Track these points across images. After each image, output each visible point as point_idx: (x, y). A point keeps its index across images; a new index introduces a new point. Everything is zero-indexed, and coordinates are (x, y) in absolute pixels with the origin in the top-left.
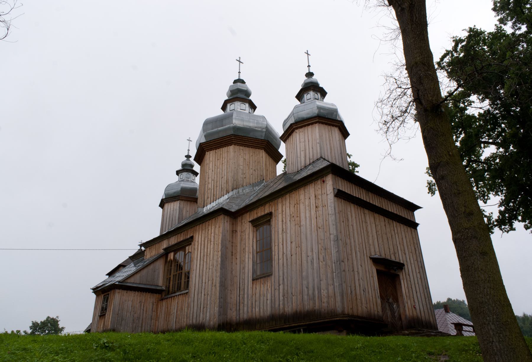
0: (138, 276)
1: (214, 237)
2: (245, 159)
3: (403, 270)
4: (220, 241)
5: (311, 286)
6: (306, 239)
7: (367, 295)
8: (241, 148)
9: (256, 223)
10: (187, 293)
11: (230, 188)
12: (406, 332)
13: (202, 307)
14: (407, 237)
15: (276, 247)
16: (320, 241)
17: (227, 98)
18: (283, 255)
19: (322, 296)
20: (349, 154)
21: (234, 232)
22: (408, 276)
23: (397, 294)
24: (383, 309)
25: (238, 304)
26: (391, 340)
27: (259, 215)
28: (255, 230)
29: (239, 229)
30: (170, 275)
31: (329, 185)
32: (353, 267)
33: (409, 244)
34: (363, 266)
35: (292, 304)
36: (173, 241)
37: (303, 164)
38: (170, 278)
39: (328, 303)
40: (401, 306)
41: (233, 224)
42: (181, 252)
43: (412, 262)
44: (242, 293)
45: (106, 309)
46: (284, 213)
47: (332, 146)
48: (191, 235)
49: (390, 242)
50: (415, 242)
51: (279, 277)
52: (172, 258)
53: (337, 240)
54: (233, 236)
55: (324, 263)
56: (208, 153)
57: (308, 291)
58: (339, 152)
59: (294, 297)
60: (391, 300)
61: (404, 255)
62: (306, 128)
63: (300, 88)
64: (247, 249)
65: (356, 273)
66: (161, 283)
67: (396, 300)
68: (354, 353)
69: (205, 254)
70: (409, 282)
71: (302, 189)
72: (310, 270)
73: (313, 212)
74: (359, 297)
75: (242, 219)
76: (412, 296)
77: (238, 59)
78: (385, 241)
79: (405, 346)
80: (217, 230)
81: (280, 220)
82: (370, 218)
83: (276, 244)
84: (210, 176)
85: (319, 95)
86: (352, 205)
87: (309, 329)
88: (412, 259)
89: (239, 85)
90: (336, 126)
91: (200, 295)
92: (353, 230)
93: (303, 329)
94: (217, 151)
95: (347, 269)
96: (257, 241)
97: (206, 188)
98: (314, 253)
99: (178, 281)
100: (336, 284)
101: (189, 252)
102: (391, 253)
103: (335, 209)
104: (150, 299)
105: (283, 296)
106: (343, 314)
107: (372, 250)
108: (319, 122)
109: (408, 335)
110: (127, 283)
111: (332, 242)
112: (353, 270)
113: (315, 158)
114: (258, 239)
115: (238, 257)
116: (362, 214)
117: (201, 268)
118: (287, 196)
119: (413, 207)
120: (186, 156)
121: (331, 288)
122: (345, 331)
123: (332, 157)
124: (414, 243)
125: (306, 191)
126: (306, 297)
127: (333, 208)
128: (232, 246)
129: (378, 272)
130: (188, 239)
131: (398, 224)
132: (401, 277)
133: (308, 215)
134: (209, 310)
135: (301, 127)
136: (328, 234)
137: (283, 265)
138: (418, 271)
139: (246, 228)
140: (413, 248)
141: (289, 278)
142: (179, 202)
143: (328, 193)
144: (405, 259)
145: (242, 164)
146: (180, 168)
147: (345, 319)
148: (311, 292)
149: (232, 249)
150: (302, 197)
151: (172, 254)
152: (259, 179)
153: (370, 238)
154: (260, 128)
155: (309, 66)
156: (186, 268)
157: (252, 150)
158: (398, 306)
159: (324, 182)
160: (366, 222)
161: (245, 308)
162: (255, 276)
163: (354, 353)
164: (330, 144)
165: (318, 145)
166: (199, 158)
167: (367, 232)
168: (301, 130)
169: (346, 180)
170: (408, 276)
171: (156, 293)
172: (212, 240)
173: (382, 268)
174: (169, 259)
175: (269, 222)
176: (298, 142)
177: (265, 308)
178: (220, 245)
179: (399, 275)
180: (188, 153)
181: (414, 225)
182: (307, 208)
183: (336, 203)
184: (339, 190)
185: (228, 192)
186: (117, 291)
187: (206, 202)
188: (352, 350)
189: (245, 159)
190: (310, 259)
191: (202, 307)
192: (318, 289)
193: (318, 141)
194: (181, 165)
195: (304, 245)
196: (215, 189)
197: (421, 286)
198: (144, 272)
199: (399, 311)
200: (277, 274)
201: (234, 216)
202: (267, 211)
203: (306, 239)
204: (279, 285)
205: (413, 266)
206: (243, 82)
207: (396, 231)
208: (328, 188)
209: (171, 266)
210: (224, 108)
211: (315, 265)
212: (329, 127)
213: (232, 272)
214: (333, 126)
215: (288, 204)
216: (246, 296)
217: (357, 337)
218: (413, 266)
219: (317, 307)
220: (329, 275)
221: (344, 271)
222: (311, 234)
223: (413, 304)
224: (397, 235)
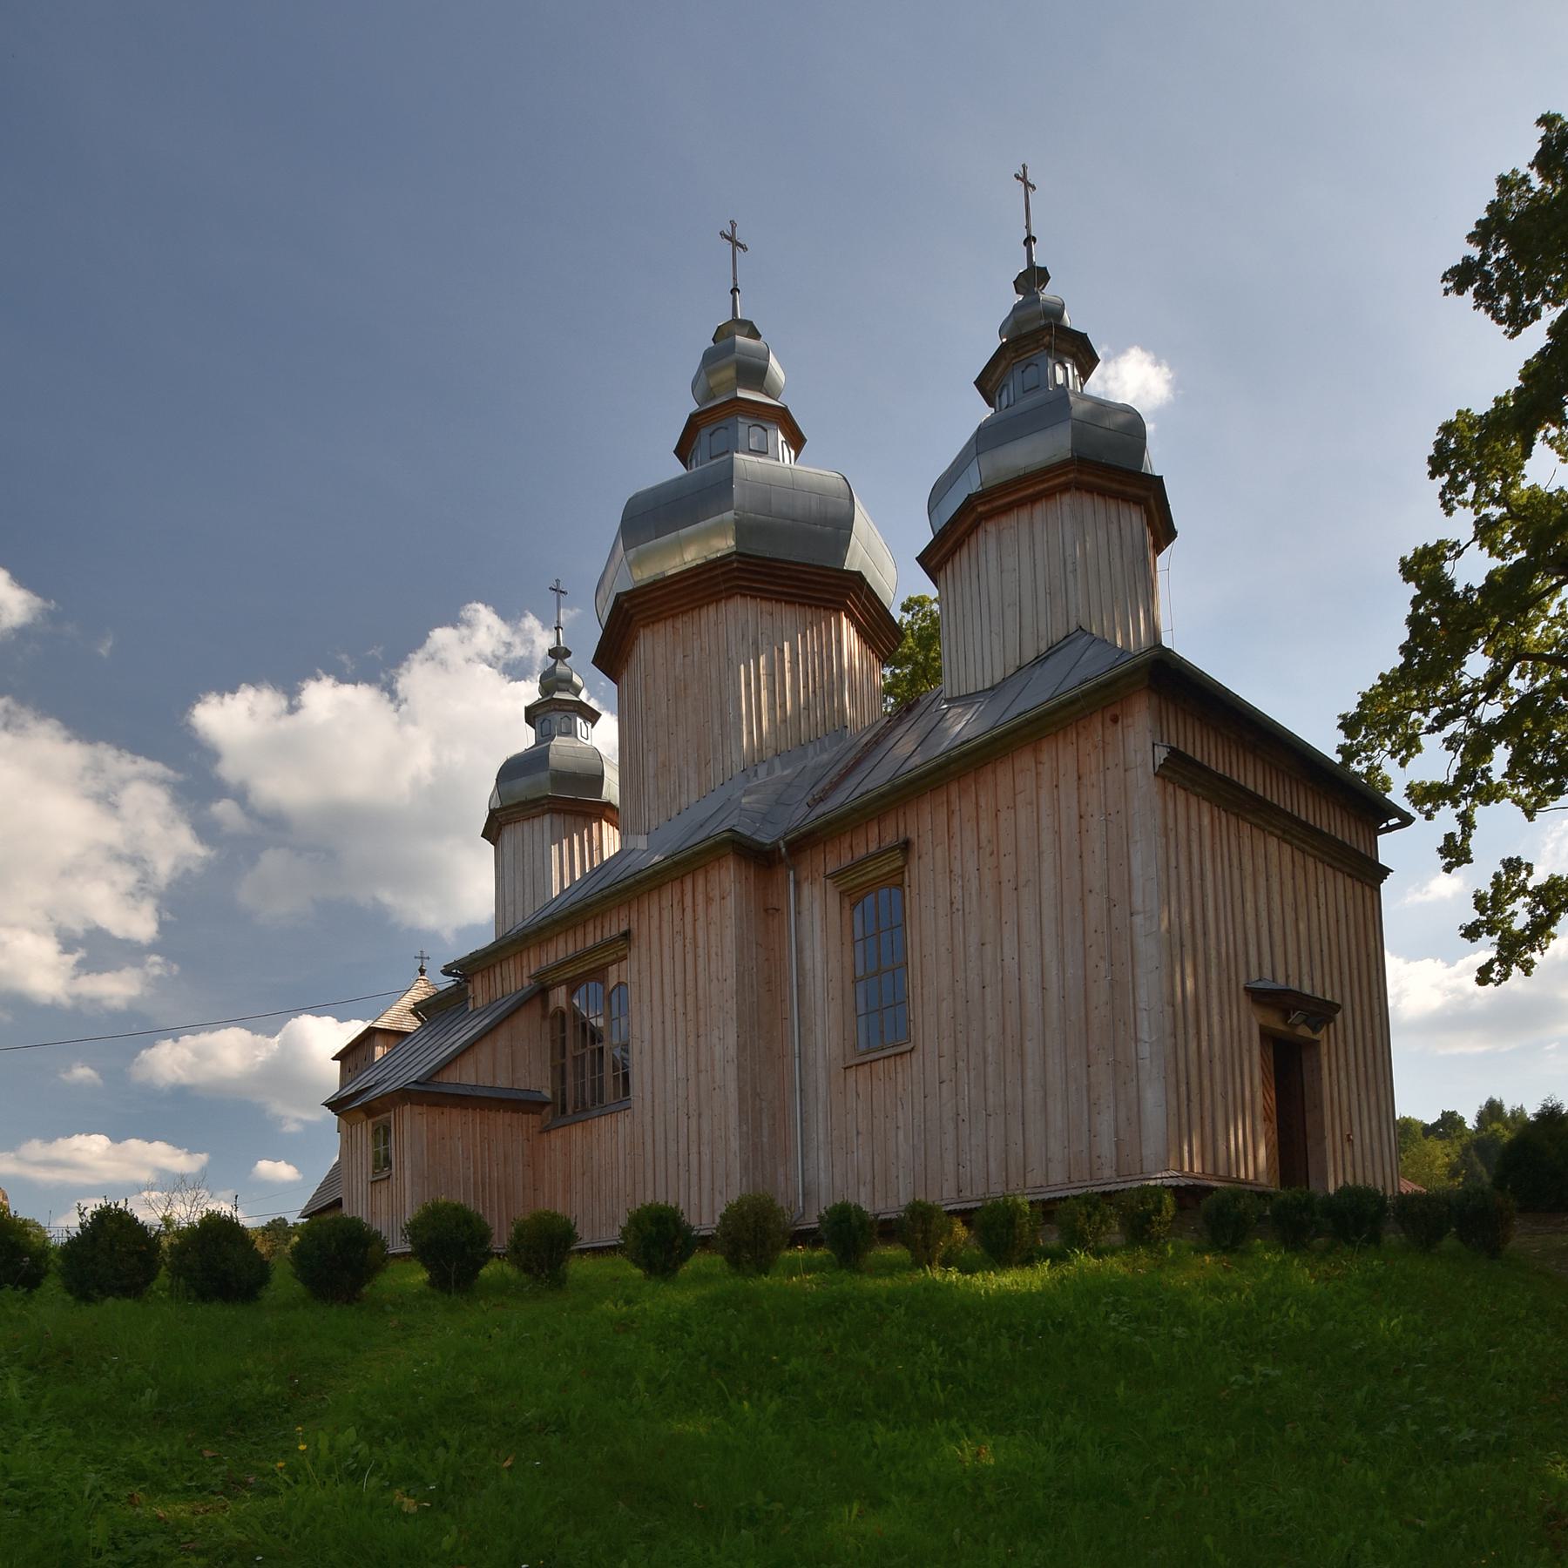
8: (766, 606)
9: (854, 888)
27: (861, 852)
30: (564, 1056)
36: (561, 949)
38: (563, 1065)
48: (624, 928)
56: (648, 632)
63: (995, 342)
66: (536, 1078)
77: (728, 232)
99: (587, 1078)
101: (619, 984)
108: (1081, 487)
130: (614, 941)
142: (547, 818)
155: (1030, 240)
156: (611, 1043)
174: (551, 1009)
175: (897, 880)
201: (764, 860)
202: (889, 839)
209: (563, 1031)
210: (684, 451)
212: (1112, 504)
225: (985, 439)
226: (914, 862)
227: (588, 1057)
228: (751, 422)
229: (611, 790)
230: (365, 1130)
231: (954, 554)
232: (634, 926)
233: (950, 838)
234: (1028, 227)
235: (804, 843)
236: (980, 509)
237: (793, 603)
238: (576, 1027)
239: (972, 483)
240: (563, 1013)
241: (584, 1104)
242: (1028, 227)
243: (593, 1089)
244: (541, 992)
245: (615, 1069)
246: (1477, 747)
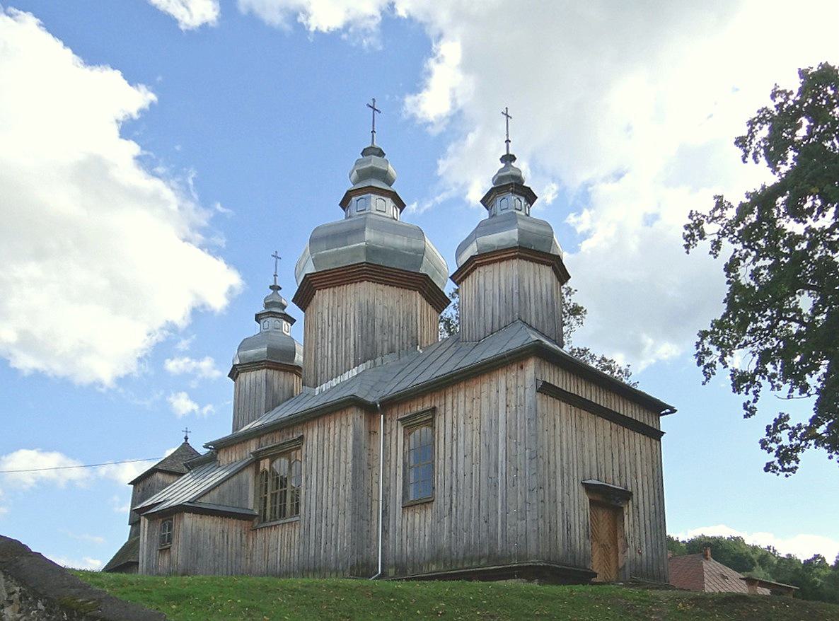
0: (215, 493)
8: (380, 286)
9: (410, 424)
17: (350, 186)
31: (531, 371)
38: (266, 498)
41: (370, 421)
42: (283, 459)
43: (646, 489)
45: (170, 540)
46: (455, 410)
49: (616, 460)
52: (267, 468)
54: (370, 439)
63: (490, 186)
71: (487, 376)
80: (346, 429)
85: (523, 199)
89: (375, 162)
90: (548, 265)
94: (336, 289)
99: (279, 502)
102: (615, 476)
104: (234, 527)
108: (521, 258)
114: (412, 447)
118: (462, 385)
119: (657, 408)
120: (271, 287)
122: (537, 580)
131: (632, 433)
135: (488, 263)
136: (523, 448)
138: (652, 502)
144: (635, 486)
146: (261, 309)
151: (267, 461)
154: (414, 250)
159: (522, 368)
166: (304, 298)
173: (597, 497)
174: (261, 469)
175: (431, 423)
181: (657, 435)
184: (544, 382)
185: (356, 364)
186: (186, 515)
192: (502, 523)
194: (123, 141)
201: (370, 410)
202: (427, 405)
207: (627, 443)
214: (543, 263)
215: (462, 398)
224: (627, 449)
225: (483, 228)
226: (437, 417)
227: (279, 494)
228: (378, 197)
229: (299, 358)
230: (603, 515)
231: (466, 278)
232: (305, 434)
233: (453, 409)
234: (507, 135)
235: (389, 404)
236: (476, 262)
237: (394, 286)
238: (273, 479)
239: (472, 250)
240: (267, 472)
241: (275, 517)
242: (507, 135)
243: (280, 510)
244: (255, 461)
245: (292, 501)
246: (765, 357)
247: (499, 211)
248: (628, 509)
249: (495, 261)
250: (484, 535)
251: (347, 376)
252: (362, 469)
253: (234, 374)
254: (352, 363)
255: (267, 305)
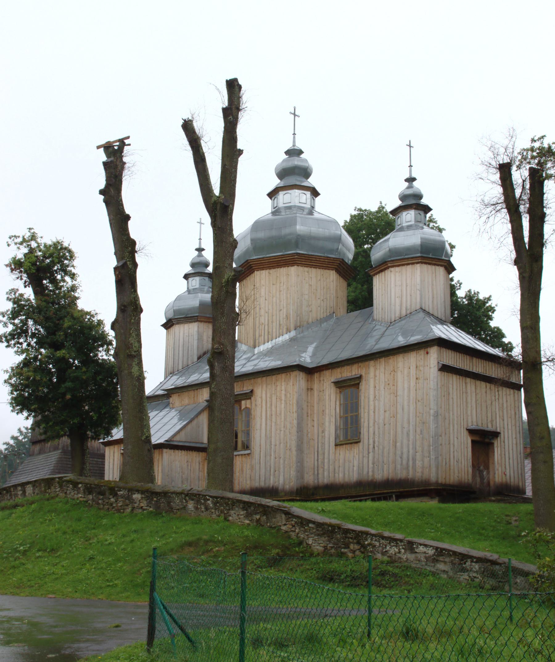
0: (183, 433)
1: (285, 395)
2: (310, 285)
3: (499, 438)
4: (295, 401)
5: (405, 456)
6: (403, 410)
7: (458, 463)
9: (340, 385)
10: (248, 454)
11: (292, 326)
12: (493, 498)
13: (272, 470)
14: (509, 401)
15: (366, 414)
16: (418, 414)
18: (374, 423)
19: (417, 466)
20: (441, 227)
21: (310, 389)
22: (502, 443)
23: (489, 462)
24: (474, 476)
25: (316, 469)
26: (480, 506)
28: (338, 392)
29: (316, 386)
32: (449, 441)
33: (509, 408)
34: (459, 438)
35: (383, 471)
37: (397, 315)
39: (422, 473)
40: (491, 473)
41: (308, 381)
43: (510, 427)
44: (321, 457)
46: (377, 378)
47: (435, 292)
50: (517, 405)
51: (369, 445)
53: (436, 415)
54: (308, 394)
55: (421, 436)
57: (402, 461)
58: (443, 300)
59: (385, 466)
60: (482, 468)
61: (501, 420)
62: (404, 267)
64: (327, 411)
65: (452, 446)
67: (487, 468)
68: (458, 515)
69: (274, 413)
70: (503, 449)
72: (405, 441)
73: (413, 383)
74: (452, 468)
75: (320, 377)
76: (503, 463)
78: (484, 409)
79: (490, 511)
81: (372, 385)
82: (470, 385)
83: (366, 411)
84: (262, 306)
86: (454, 376)
87: (400, 496)
88: (510, 424)
90: (441, 266)
91: (268, 458)
92: (453, 403)
93: (396, 496)
95: (444, 443)
96: (340, 405)
97: (257, 323)
98: (411, 425)
100: (433, 457)
102: (489, 421)
103: (437, 384)
105: (373, 464)
106: (437, 483)
107: (470, 421)
108: (422, 263)
109: (494, 501)
110: (173, 441)
111: (432, 418)
112: (449, 443)
113: (413, 308)
115: (315, 419)
116: (464, 384)
117: (268, 428)
121: (426, 460)
123: (433, 308)
124: (515, 407)
125: (406, 358)
126: (399, 467)
127: (436, 383)
128: (308, 406)
129: (473, 442)
132: (495, 445)
133: (406, 386)
134: (282, 474)
137: (374, 433)
138: (514, 436)
139: (325, 387)
140: (513, 413)
141: (381, 447)
143: (432, 366)
145: (307, 293)
146: (188, 269)
147: (439, 488)
148: (405, 462)
149: (308, 410)
150: (400, 364)
152: (328, 311)
153: (469, 408)
157: (319, 271)
158: (488, 473)
159: (427, 353)
160: (466, 393)
161: (326, 473)
162: (338, 441)
163: (458, 515)
164: (433, 291)
165: (418, 292)
167: (467, 403)
168: (397, 269)
169: (451, 350)
170: (502, 443)
171: (202, 451)
172: (283, 398)
173: (476, 438)
175: (357, 386)
176: (393, 285)
177: (351, 474)
178: (295, 405)
179: (493, 444)
180: (200, 243)
182: (406, 378)
183: (439, 378)
185: (288, 331)
186: (165, 450)
187: (257, 341)
188: (456, 513)
189: (310, 285)
190: (405, 430)
191: (272, 470)
192: (413, 459)
193: (418, 287)
195: (399, 416)
196: (270, 325)
197: (515, 452)
198: (189, 427)
199: (489, 478)
200: (366, 441)
201: (310, 372)
203: (403, 410)
204: (369, 453)
205: (510, 431)
206: (300, 152)
208: (432, 362)
211: (411, 437)
212: (434, 267)
213: (307, 434)
214: (438, 265)
216: (326, 461)
217: (457, 505)
218: (510, 431)
219: (410, 476)
220: (426, 448)
221: (441, 445)
222: (409, 406)
223: (504, 470)
247: (404, 221)
248: (497, 443)
249: (398, 266)
250: (399, 467)
251: (280, 340)
252: (303, 416)
253: (168, 325)
254: (285, 330)
255: (193, 265)
